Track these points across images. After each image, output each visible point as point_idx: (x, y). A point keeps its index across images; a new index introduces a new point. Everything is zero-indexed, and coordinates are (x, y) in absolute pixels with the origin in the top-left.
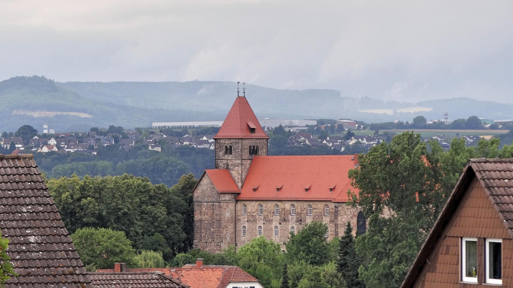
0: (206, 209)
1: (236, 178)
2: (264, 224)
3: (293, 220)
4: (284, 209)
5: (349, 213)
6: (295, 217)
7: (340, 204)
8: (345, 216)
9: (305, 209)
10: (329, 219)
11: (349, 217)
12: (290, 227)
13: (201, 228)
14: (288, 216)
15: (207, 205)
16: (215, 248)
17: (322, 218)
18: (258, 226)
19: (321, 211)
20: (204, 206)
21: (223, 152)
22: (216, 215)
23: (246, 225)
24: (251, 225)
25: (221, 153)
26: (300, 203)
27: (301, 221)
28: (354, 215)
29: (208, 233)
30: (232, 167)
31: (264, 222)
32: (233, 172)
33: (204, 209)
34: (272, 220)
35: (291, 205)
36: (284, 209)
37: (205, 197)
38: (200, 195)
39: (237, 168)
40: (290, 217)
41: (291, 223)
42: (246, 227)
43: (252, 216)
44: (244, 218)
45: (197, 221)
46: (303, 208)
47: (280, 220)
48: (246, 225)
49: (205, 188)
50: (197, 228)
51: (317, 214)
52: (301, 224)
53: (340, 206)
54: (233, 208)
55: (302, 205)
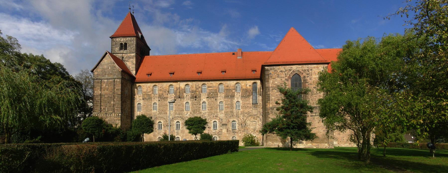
0: (106, 85)
1: (131, 68)
2: (159, 100)
3: (188, 97)
4: (179, 88)
5: (283, 75)
6: (190, 94)
7: (272, 67)
8: (279, 79)
9: (200, 87)
10: (224, 95)
11: (284, 80)
12: (184, 103)
13: (101, 101)
14: (183, 94)
15: (107, 82)
16: (115, 119)
17: (217, 94)
18: (153, 102)
19: (216, 88)
20: (104, 82)
21: (119, 48)
22: (117, 90)
23: (142, 102)
24: (146, 102)
25: (117, 49)
26: (194, 83)
27: (196, 97)
28: (289, 77)
29: (108, 105)
30: (126, 59)
31: (159, 99)
32: (128, 63)
33: (104, 85)
34: (167, 98)
35: (186, 85)
36: (179, 88)
37: (105, 75)
38: (101, 73)
39: (131, 59)
40: (185, 95)
41: (185, 99)
42: (142, 104)
43: (147, 95)
44: (139, 97)
45: (97, 96)
46: (197, 87)
47: (175, 97)
48: (142, 102)
49: (105, 67)
50: (96, 102)
51: (212, 91)
52: (196, 100)
53: (271, 69)
54: (130, 87)
55: (197, 84)
